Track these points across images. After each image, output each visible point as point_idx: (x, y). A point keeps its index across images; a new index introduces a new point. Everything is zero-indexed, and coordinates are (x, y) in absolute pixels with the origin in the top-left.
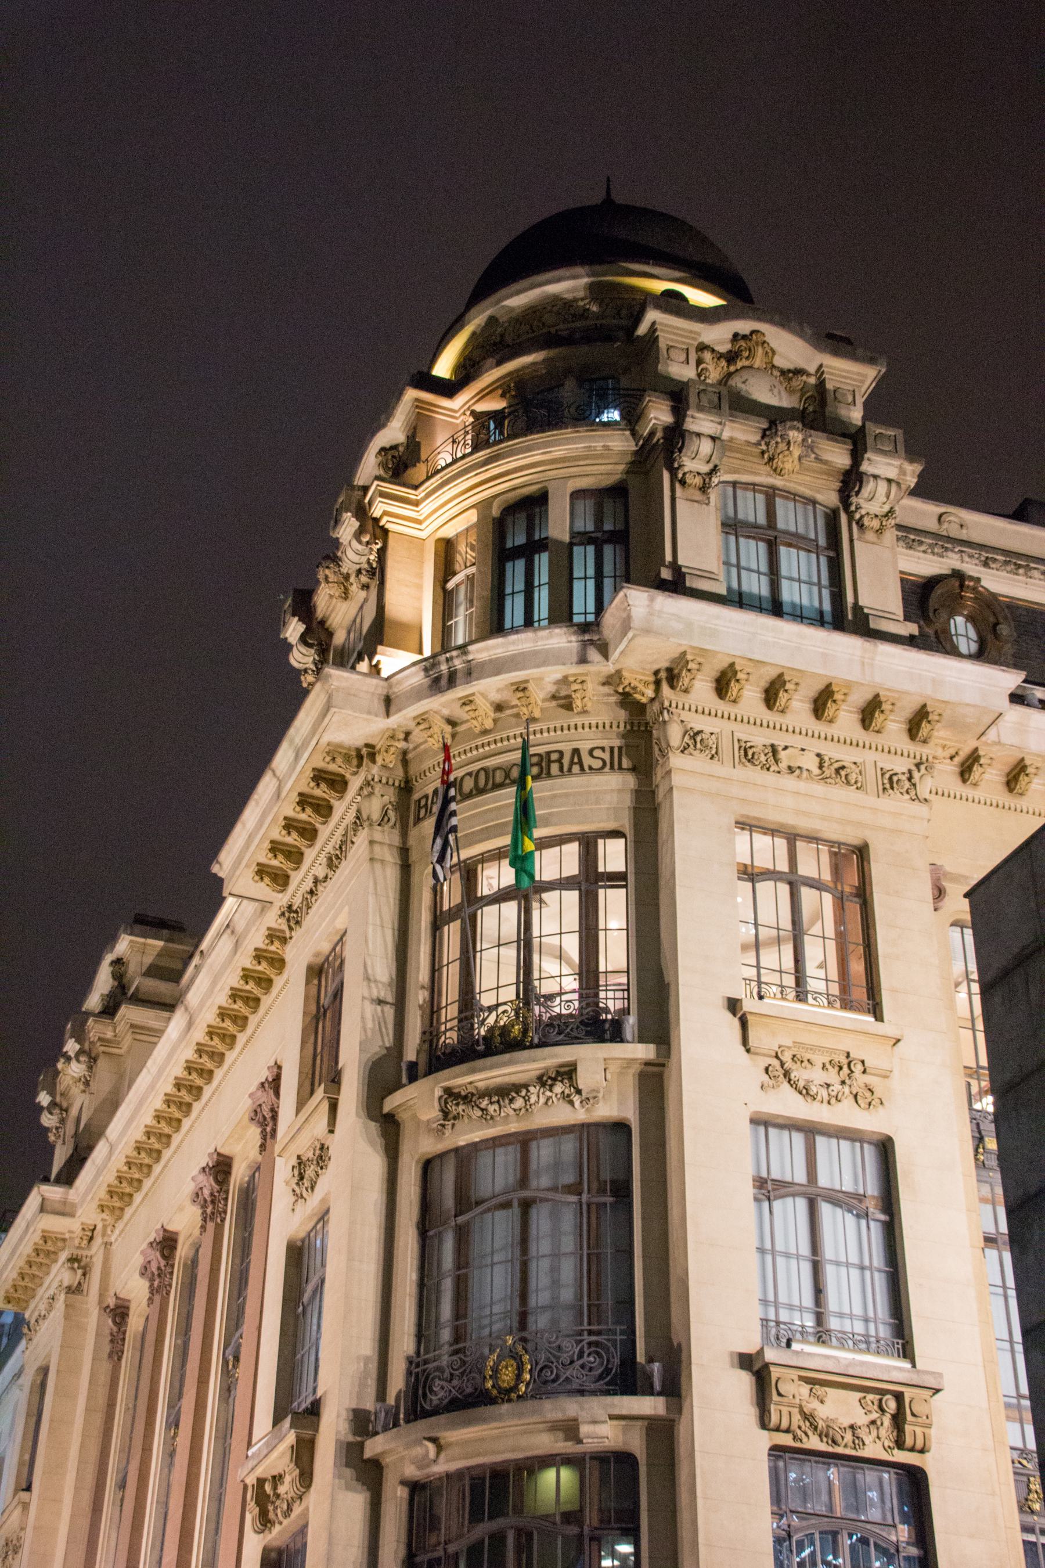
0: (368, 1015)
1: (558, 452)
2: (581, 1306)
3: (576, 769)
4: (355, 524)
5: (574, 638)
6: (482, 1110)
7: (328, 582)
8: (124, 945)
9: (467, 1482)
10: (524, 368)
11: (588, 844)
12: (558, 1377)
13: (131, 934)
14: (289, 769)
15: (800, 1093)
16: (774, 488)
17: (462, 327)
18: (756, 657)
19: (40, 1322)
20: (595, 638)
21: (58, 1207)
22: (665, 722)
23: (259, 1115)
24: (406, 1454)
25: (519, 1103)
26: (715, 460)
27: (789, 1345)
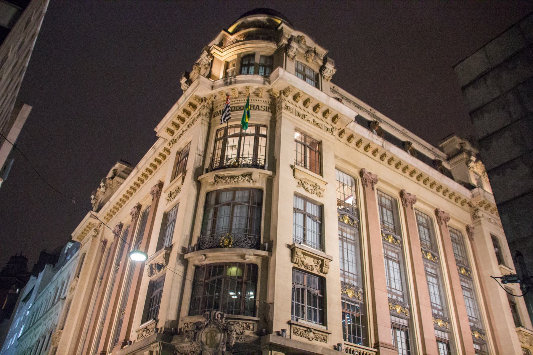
1: (259, 45)
4: (207, 53)
8: (118, 165)
9: (212, 268)
11: (258, 127)
14: (182, 102)
16: (306, 65)
24: (196, 259)
25: (236, 180)
27: (300, 243)
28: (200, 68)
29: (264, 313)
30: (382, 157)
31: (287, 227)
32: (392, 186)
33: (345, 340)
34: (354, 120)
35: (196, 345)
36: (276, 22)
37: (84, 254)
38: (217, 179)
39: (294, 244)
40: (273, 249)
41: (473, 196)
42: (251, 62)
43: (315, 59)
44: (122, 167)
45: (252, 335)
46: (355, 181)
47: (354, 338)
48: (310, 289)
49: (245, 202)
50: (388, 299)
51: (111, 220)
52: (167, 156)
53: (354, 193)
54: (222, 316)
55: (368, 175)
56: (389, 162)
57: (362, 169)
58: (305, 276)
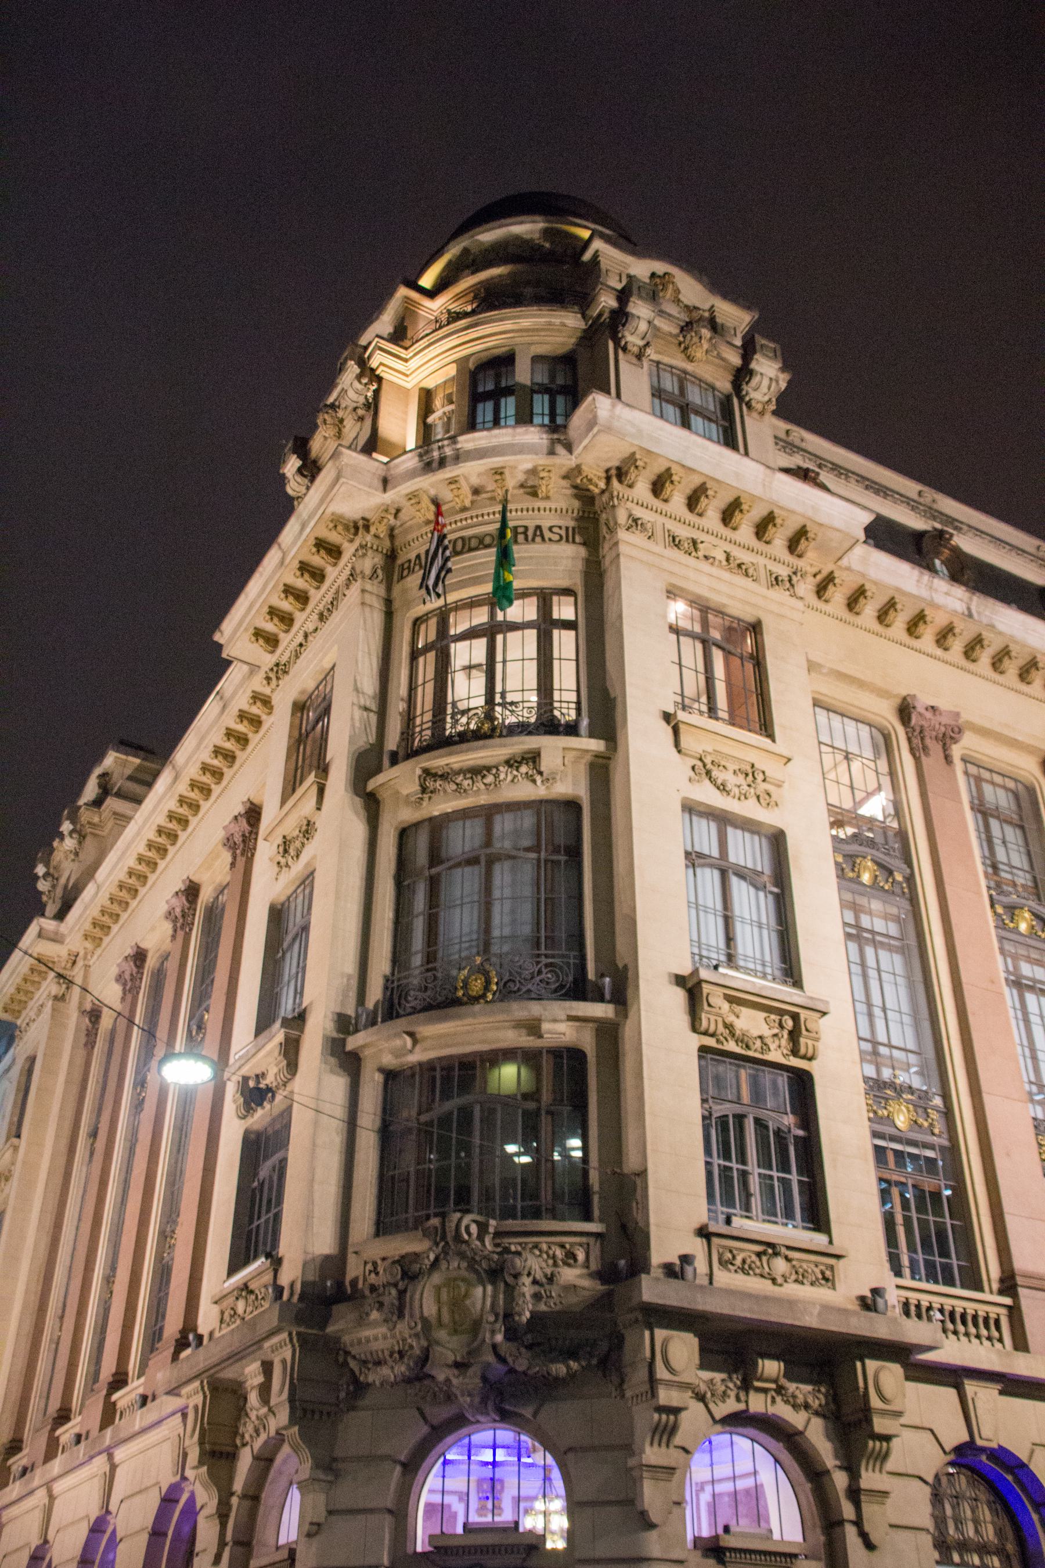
0: (357, 716)
1: (526, 323)
2: (538, 938)
3: (538, 539)
4: (357, 370)
5: (545, 436)
6: (457, 784)
7: (325, 424)
8: (111, 760)
10: (492, 278)
11: (545, 598)
12: (519, 990)
13: (117, 751)
14: (294, 539)
15: (718, 788)
16: (685, 372)
17: (442, 255)
18: (689, 463)
19: (31, 1024)
20: (562, 438)
21: (52, 936)
22: (614, 506)
23: (231, 841)
24: (385, 1047)
25: (490, 779)
26: (648, 337)
27: (716, 967)
28: (341, 421)
29: (615, 1203)
30: (971, 650)
31: (668, 916)
32: (1013, 743)
33: (898, 1273)
34: (862, 536)
35: (407, 1333)
36: (576, 238)
37: (32, 1060)
38: (430, 784)
39: (696, 972)
40: (630, 992)
42: (503, 384)
43: (714, 346)
44: (124, 764)
45: (586, 1283)
46: (887, 738)
47: (930, 1266)
48: (763, 1114)
49: (527, 850)
50: (1030, 1124)
51: (106, 940)
52: (264, 717)
53: (886, 781)
54: (483, 1228)
55: (929, 715)
56: (997, 664)
57: (905, 699)
58: (743, 1074)
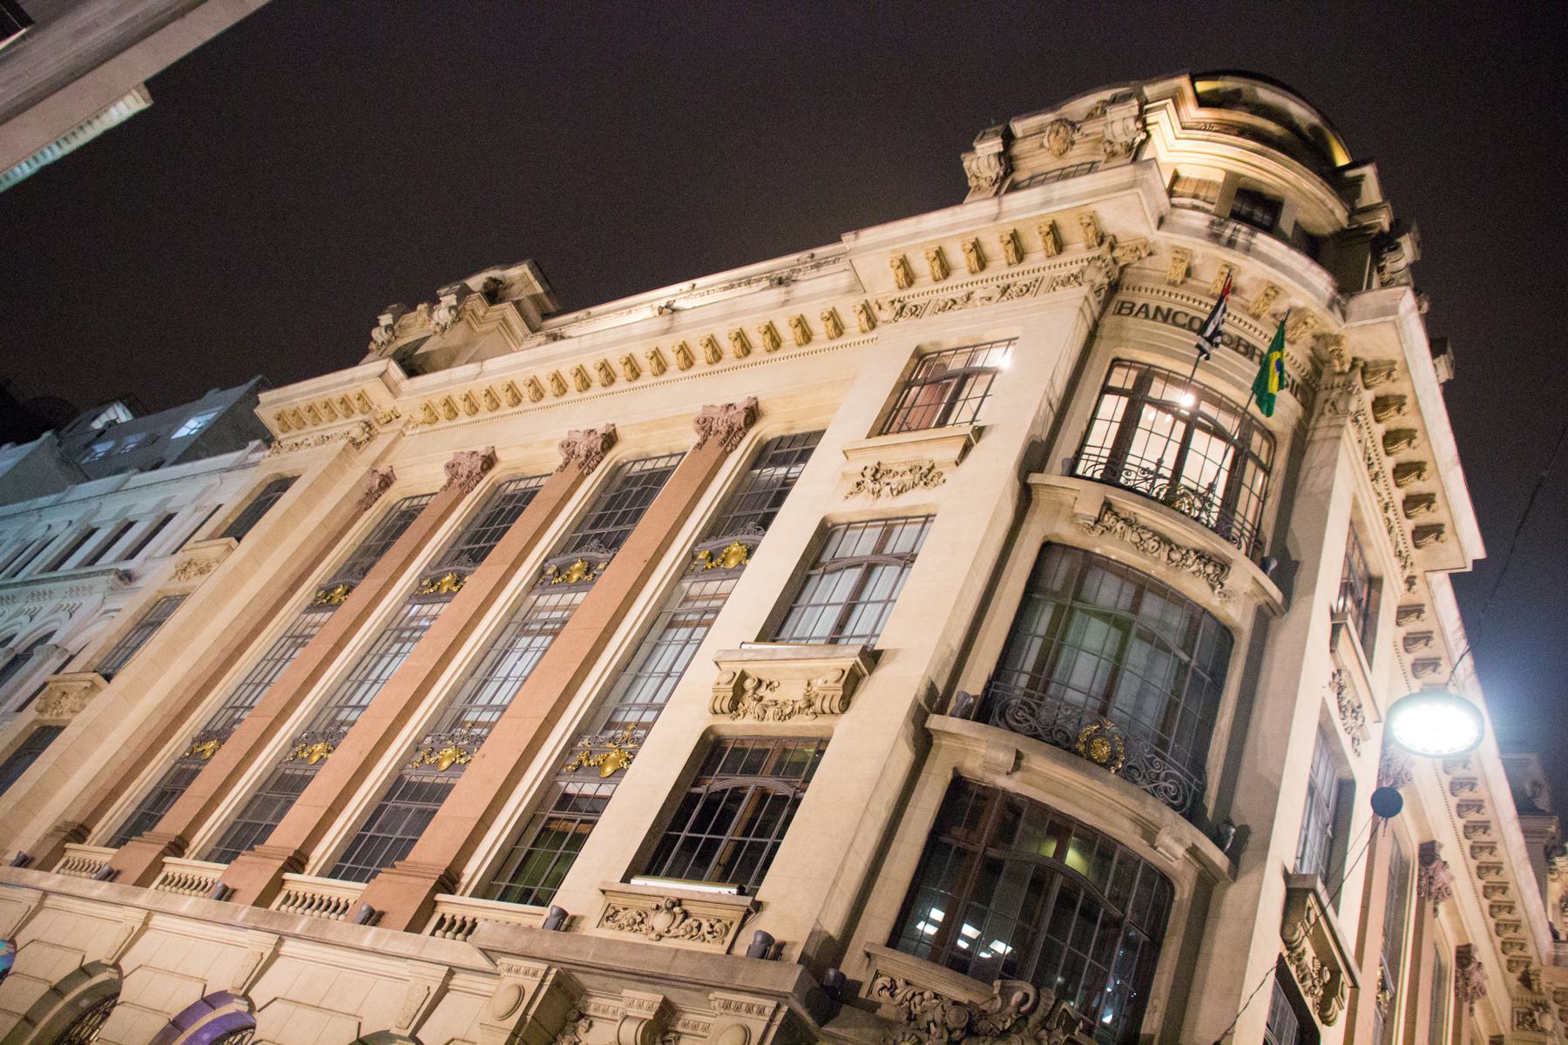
4: (1135, 111)
24: (982, 753)
25: (1176, 556)
28: (1073, 143)
38: (1109, 520)
41: (1556, 961)
